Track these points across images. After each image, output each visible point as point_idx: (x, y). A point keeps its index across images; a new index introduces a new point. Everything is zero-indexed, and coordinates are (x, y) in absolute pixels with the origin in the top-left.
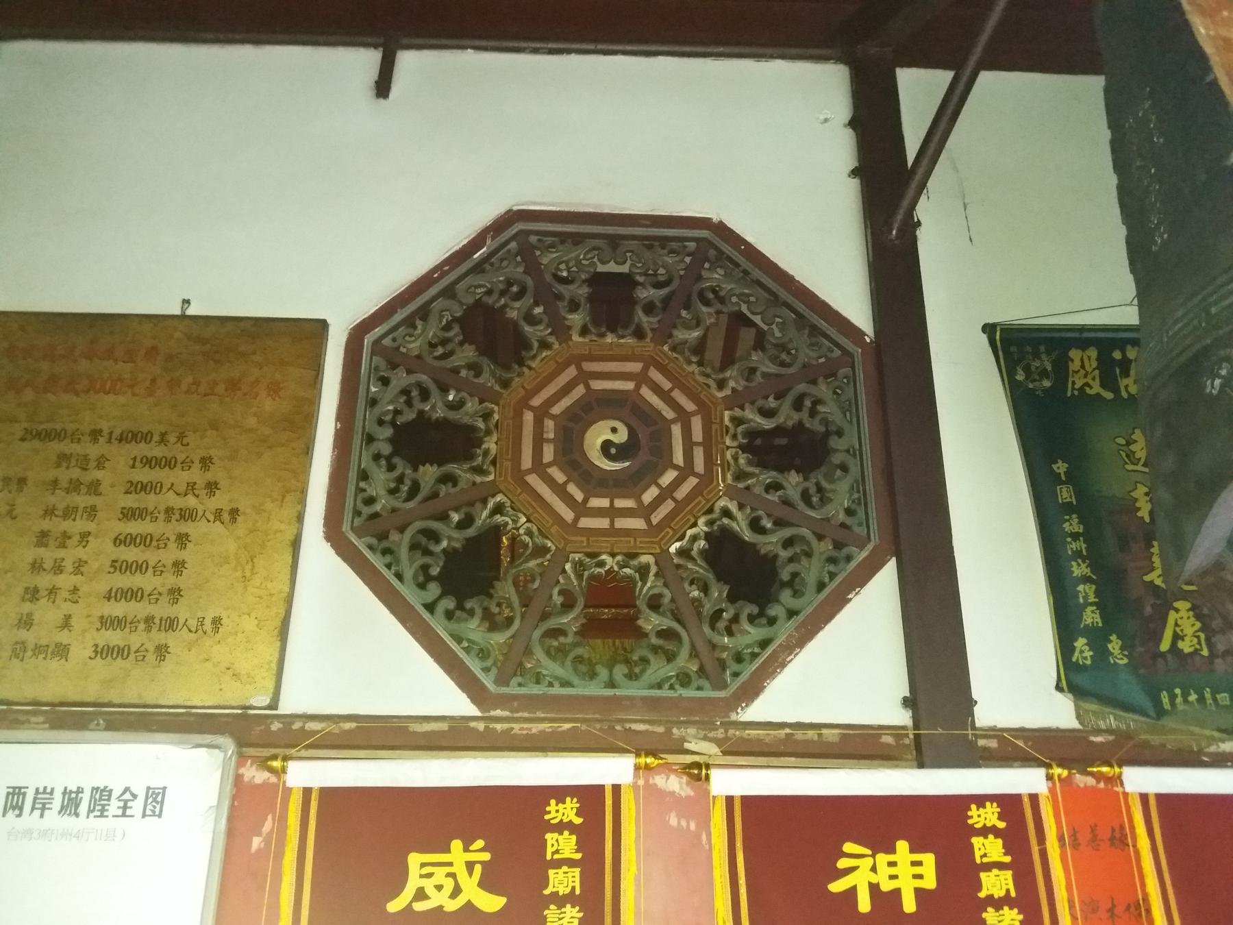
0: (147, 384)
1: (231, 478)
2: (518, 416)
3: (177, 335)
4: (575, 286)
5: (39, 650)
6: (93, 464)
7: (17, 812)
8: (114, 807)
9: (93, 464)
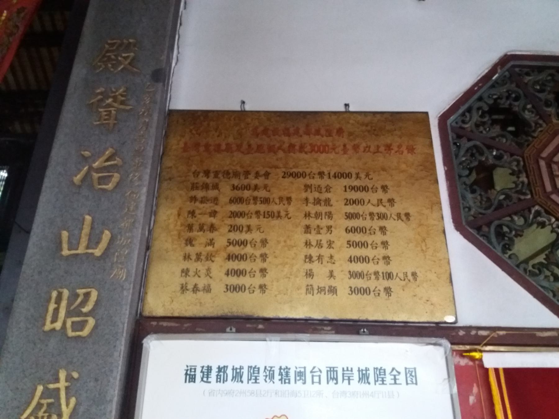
0: (342, 147)
1: (400, 197)
2: (538, 162)
3: (351, 121)
4: (546, 93)
5: (321, 290)
6: (324, 190)
7: (335, 381)
8: (389, 379)
9: (324, 190)
